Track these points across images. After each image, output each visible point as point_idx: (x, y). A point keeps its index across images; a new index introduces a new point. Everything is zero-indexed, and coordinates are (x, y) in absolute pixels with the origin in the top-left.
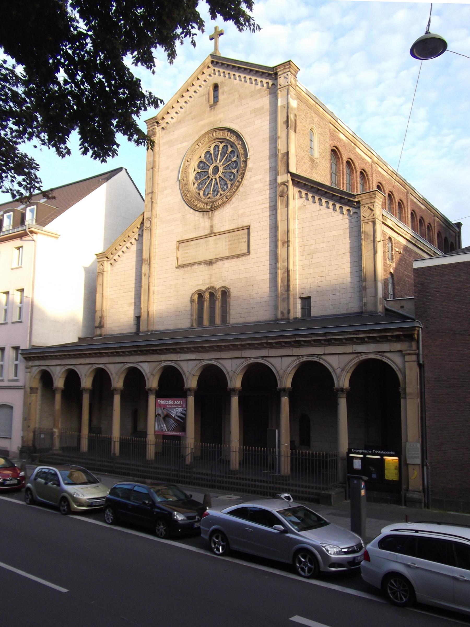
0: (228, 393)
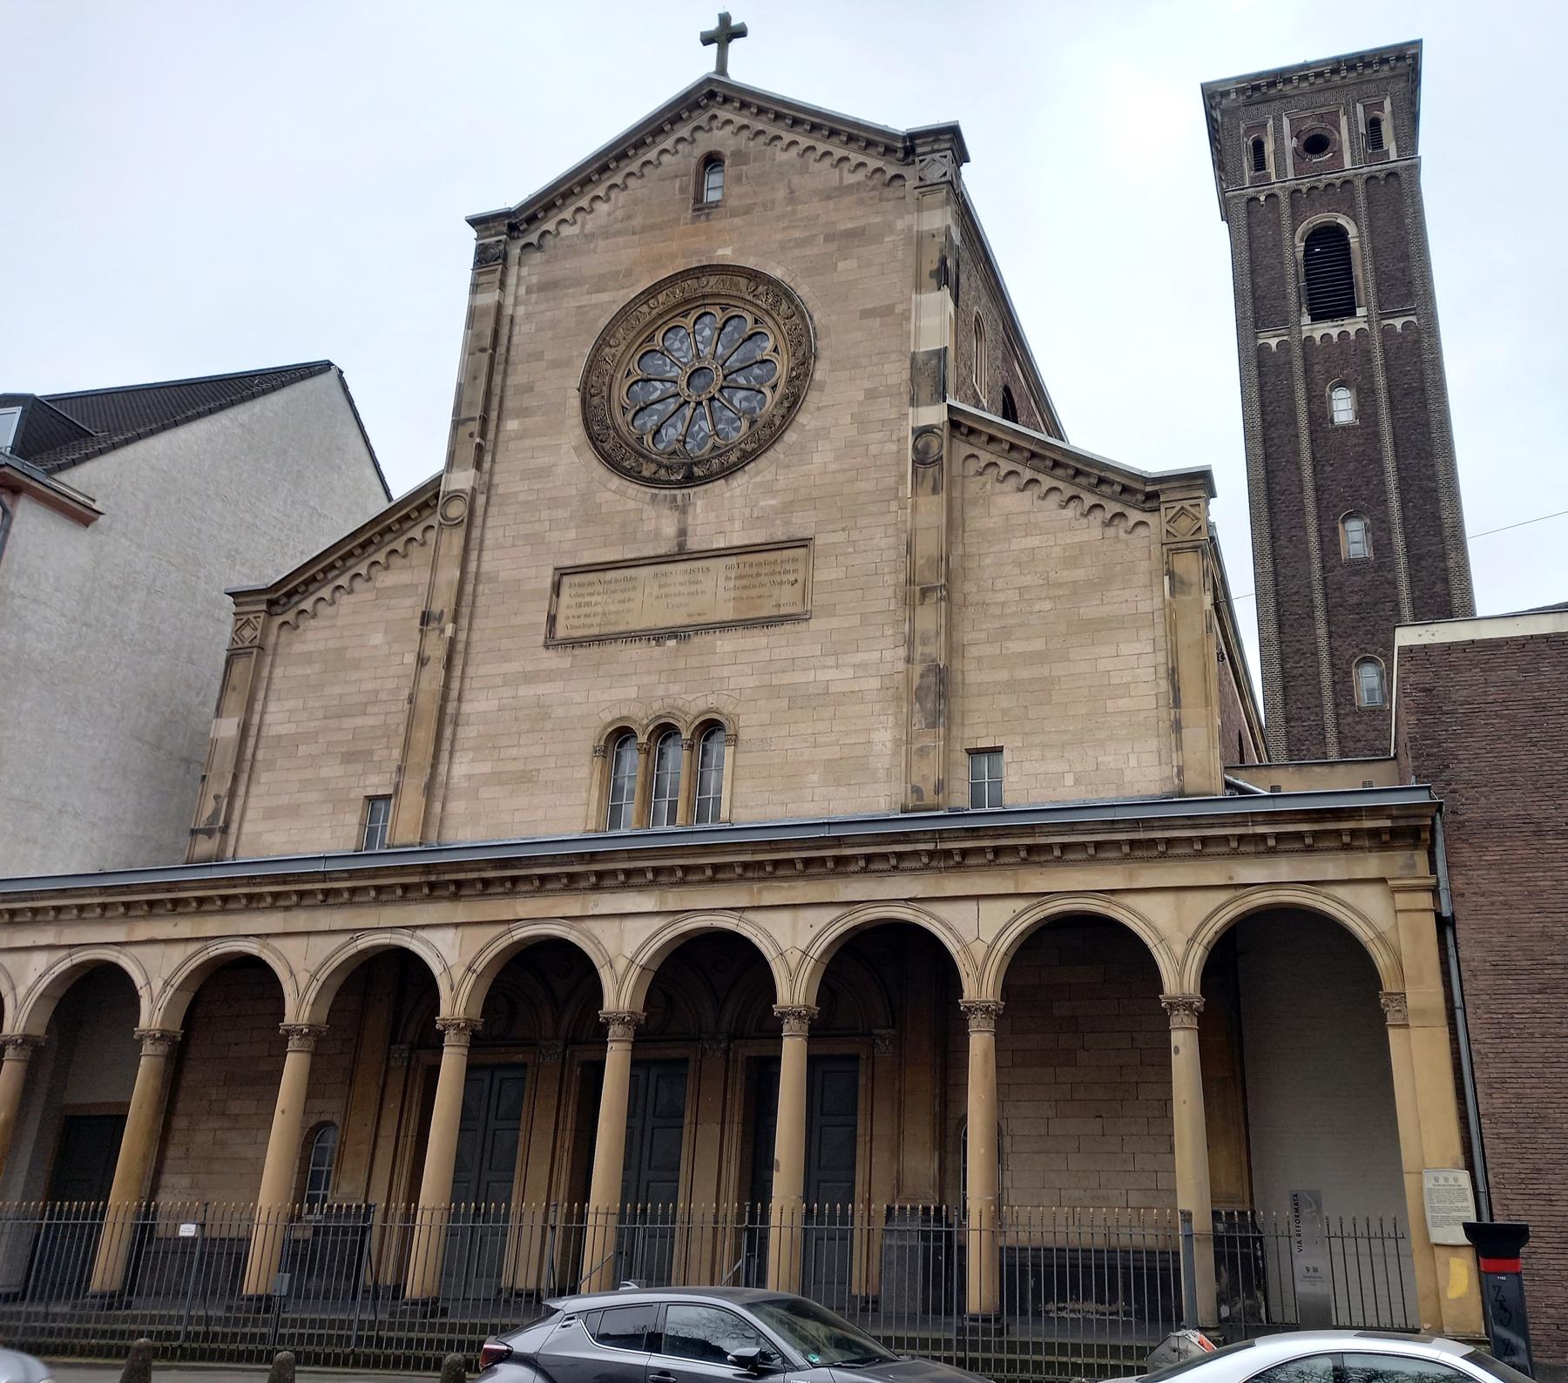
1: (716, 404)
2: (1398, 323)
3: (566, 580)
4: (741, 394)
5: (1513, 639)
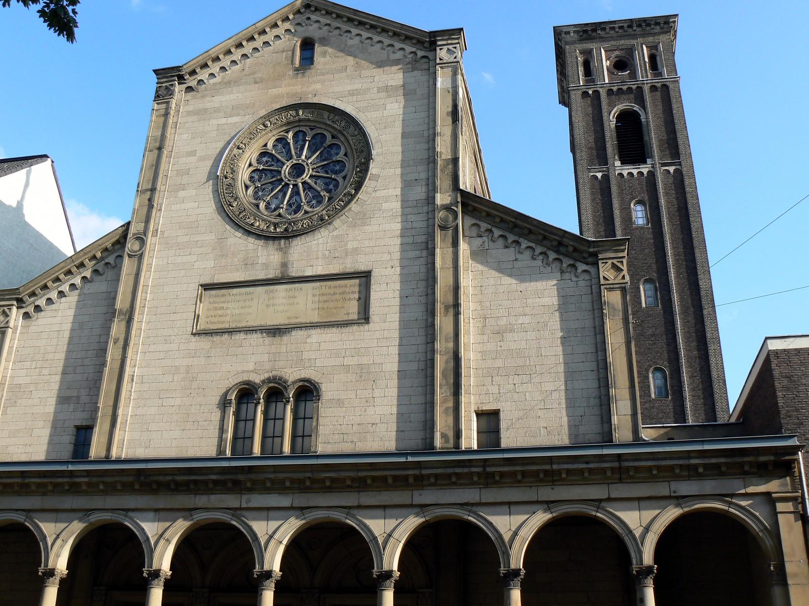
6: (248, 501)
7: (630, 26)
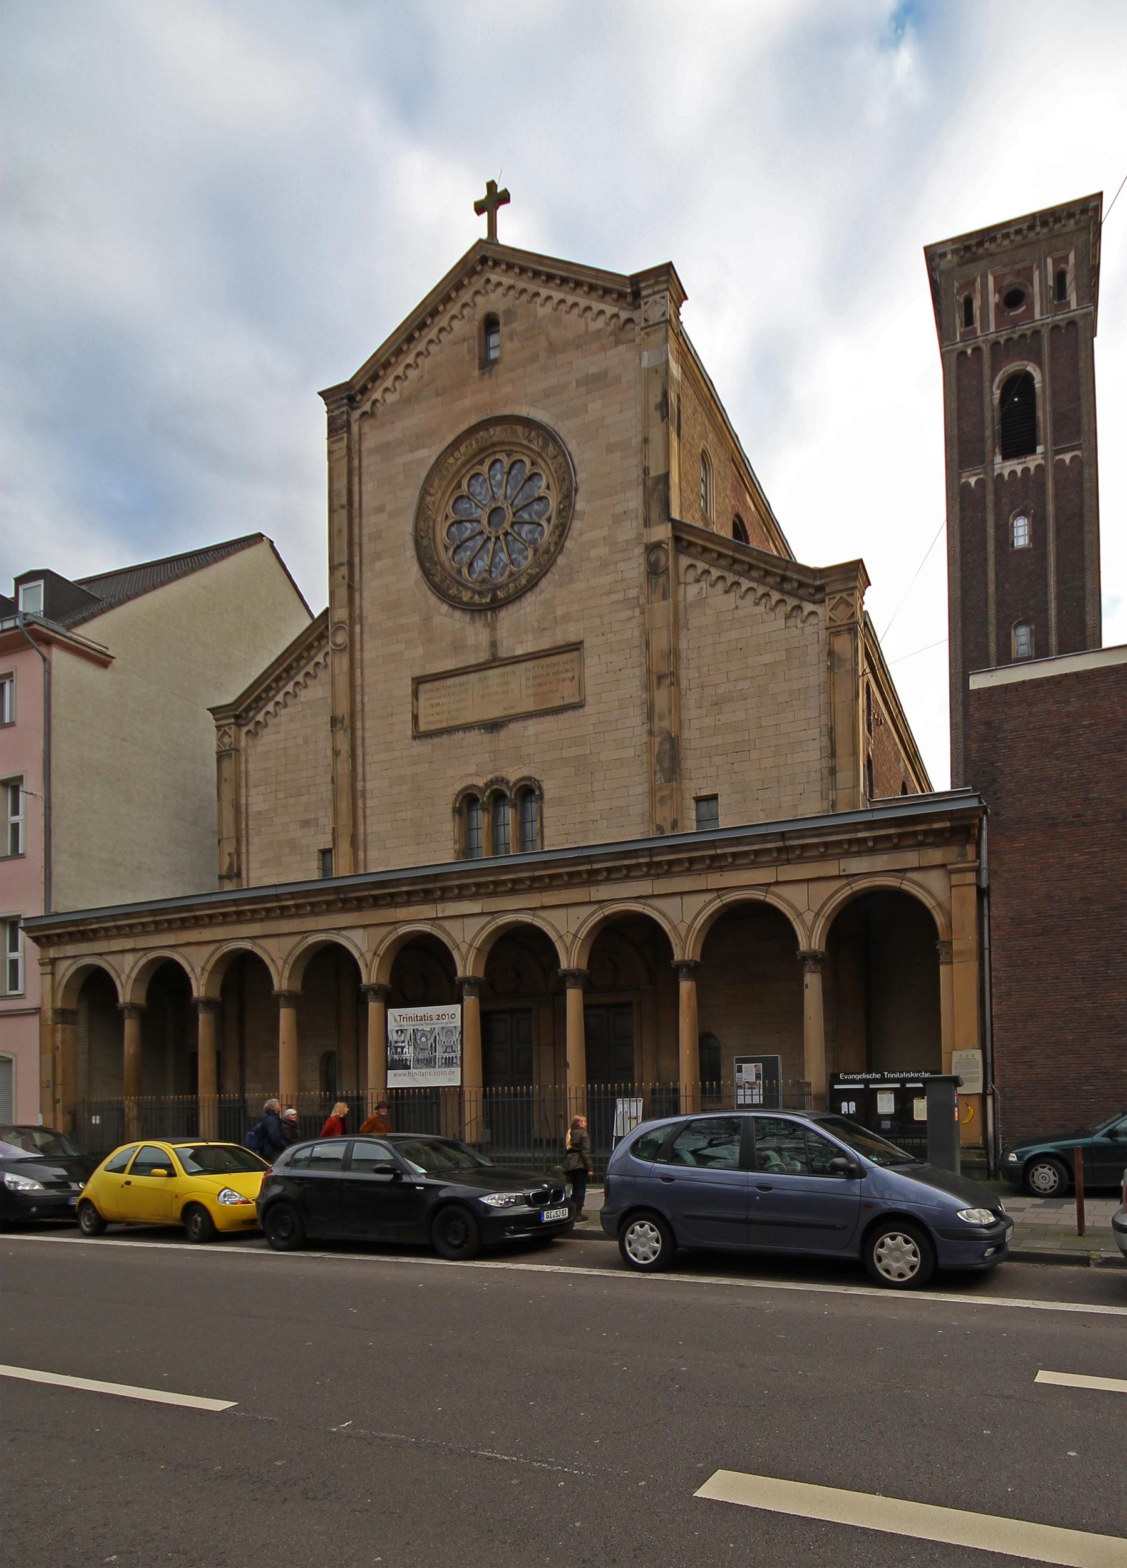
0: (559, 983)
1: (510, 538)
2: (1067, 458)
3: (422, 687)
4: (527, 528)
5: (1052, 677)
6: (443, 910)
7: (1031, 228)
